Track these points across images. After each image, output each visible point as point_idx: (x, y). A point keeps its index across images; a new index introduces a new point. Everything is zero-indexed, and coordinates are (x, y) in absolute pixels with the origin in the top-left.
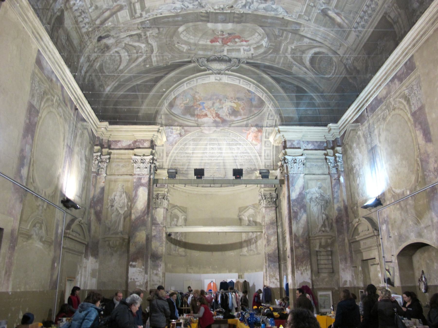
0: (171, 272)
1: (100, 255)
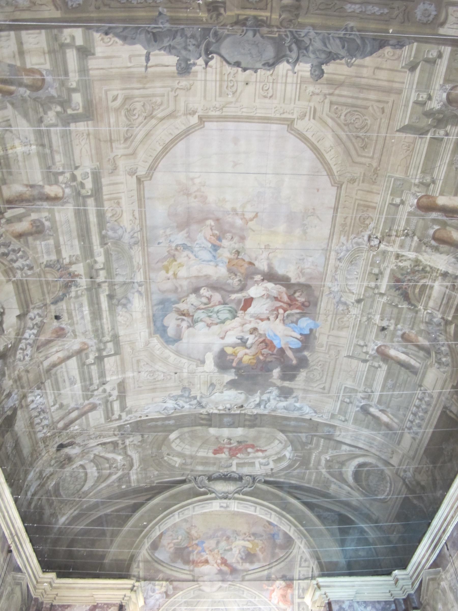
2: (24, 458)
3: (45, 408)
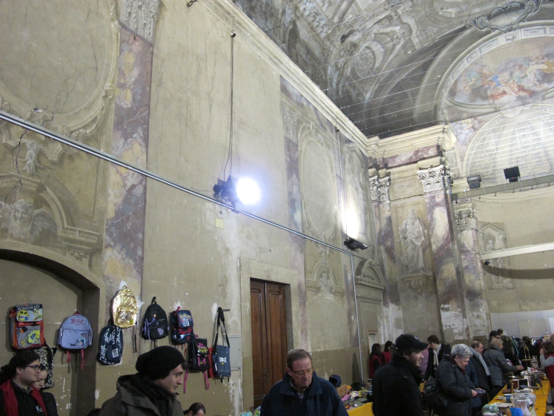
0: (498, 311)
1: (402, 300)
2: (318, 59)
3: (317, 11)
